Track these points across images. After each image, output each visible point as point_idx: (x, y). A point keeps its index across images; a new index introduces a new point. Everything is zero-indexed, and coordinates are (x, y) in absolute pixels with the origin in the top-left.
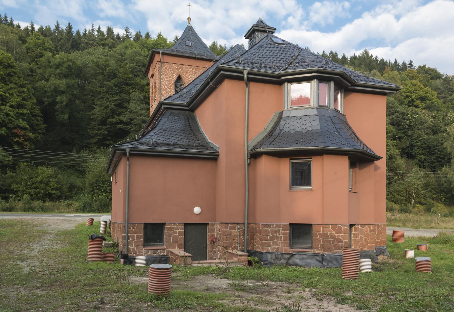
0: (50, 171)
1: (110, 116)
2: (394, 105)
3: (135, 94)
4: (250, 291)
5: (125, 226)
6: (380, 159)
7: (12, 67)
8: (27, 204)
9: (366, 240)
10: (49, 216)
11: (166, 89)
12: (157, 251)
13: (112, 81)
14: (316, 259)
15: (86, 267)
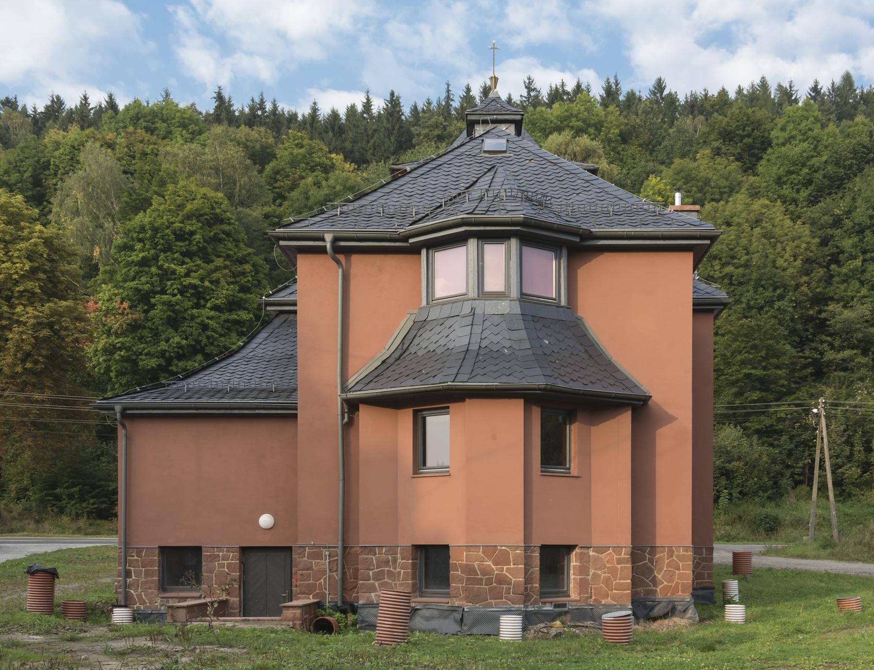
7: (222, 221)
9: (607, 581)
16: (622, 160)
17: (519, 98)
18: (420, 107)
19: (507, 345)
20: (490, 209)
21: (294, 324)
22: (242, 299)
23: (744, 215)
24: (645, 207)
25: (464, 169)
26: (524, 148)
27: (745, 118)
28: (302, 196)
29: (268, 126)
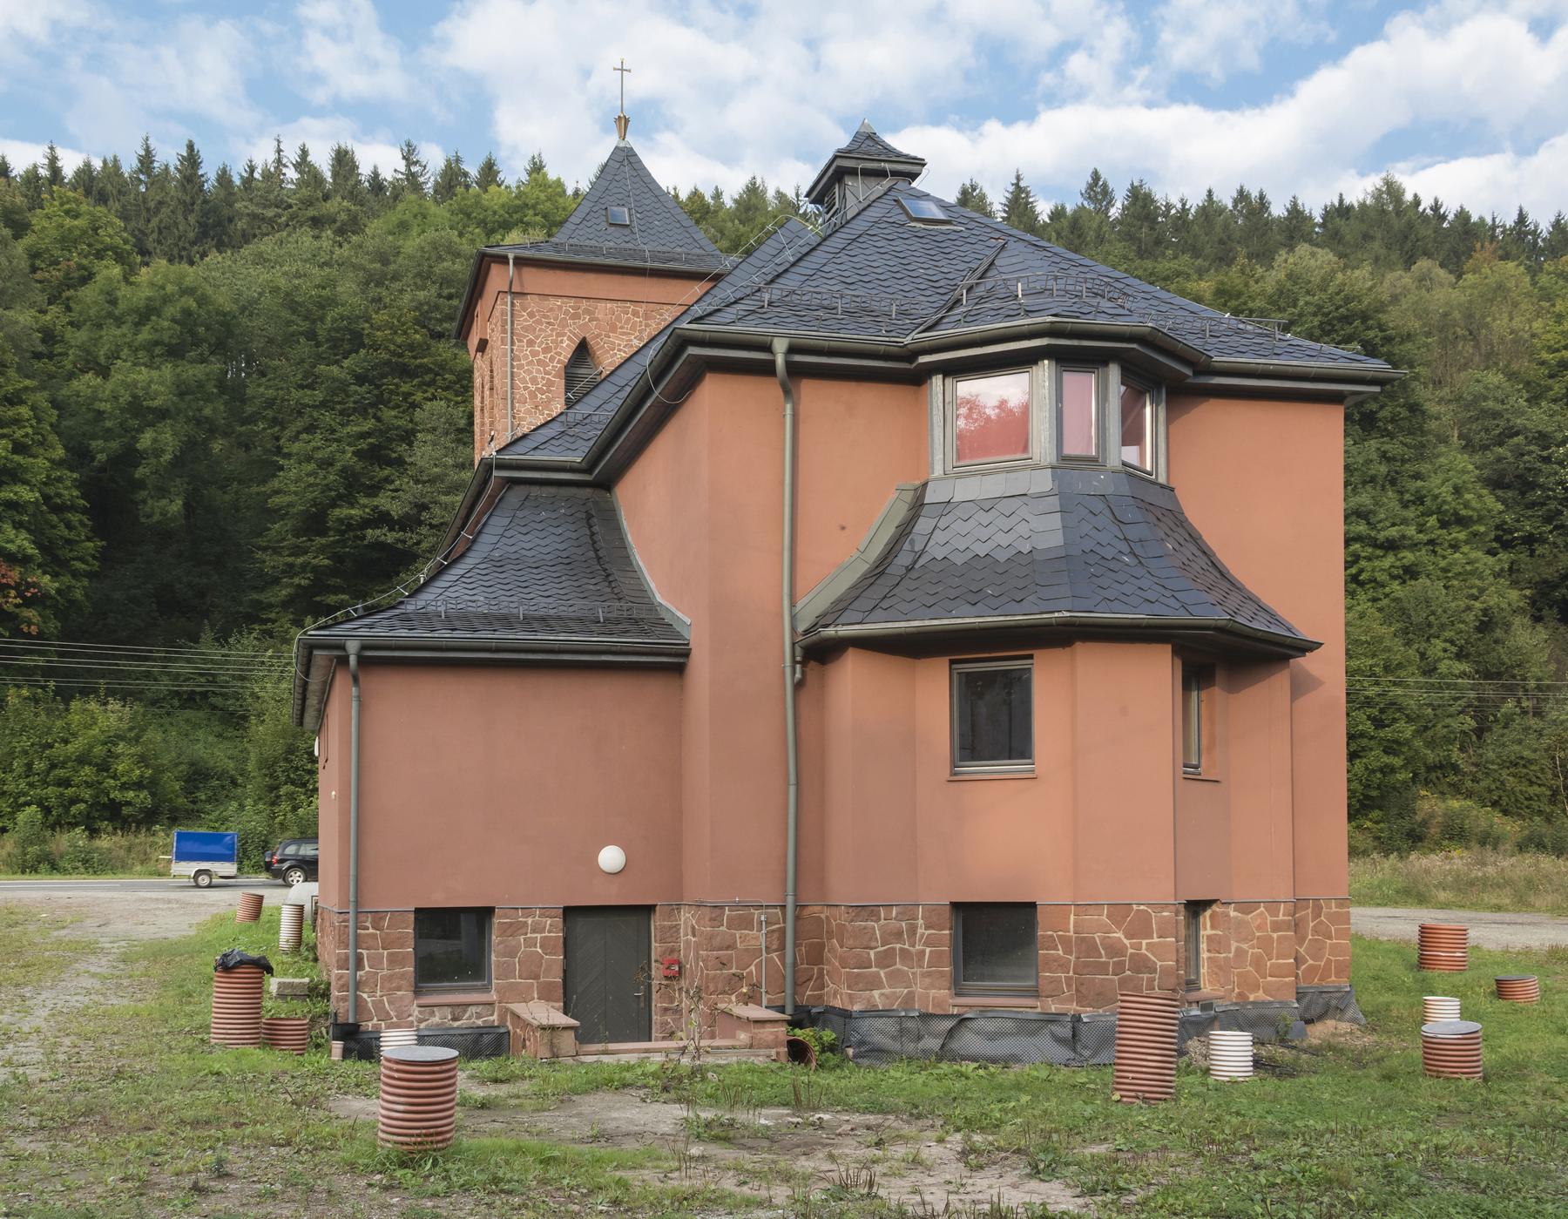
0: (111, 716)
1: (340, 497)
2: (1503, 403)
3: (434, 410)
4: (749, 1142)
5: (347, 921)
6: (1311, 650)
8: (32, 843)
9: (1258, 963)
10: (109, 889)
11: (533, 395)
12: (465, 1011)
13: (346, 363)
14: (1053, 1035)
15: (199, 1065)
22: (19, 464)
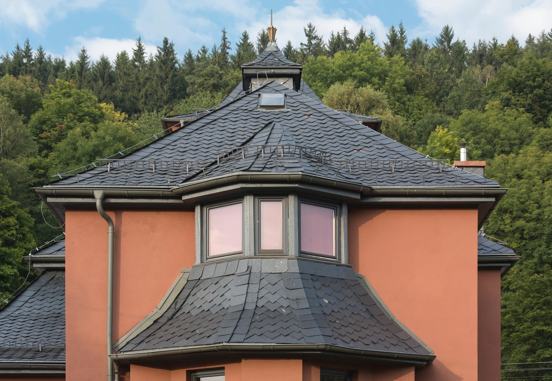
16: (407, 111)
17: (300, 46)
18: (195, 54)
19: (285, 305)
20: (267, 166)
21: (61, 282)
22: (5, 253)
23: (535, 167)
24: (429, 164)
25: (240, 124)
26: (302, 103)
27: (535, 69)
28: (70, 146)
29: (34, 74)
